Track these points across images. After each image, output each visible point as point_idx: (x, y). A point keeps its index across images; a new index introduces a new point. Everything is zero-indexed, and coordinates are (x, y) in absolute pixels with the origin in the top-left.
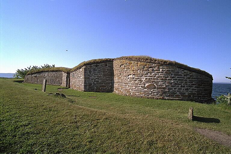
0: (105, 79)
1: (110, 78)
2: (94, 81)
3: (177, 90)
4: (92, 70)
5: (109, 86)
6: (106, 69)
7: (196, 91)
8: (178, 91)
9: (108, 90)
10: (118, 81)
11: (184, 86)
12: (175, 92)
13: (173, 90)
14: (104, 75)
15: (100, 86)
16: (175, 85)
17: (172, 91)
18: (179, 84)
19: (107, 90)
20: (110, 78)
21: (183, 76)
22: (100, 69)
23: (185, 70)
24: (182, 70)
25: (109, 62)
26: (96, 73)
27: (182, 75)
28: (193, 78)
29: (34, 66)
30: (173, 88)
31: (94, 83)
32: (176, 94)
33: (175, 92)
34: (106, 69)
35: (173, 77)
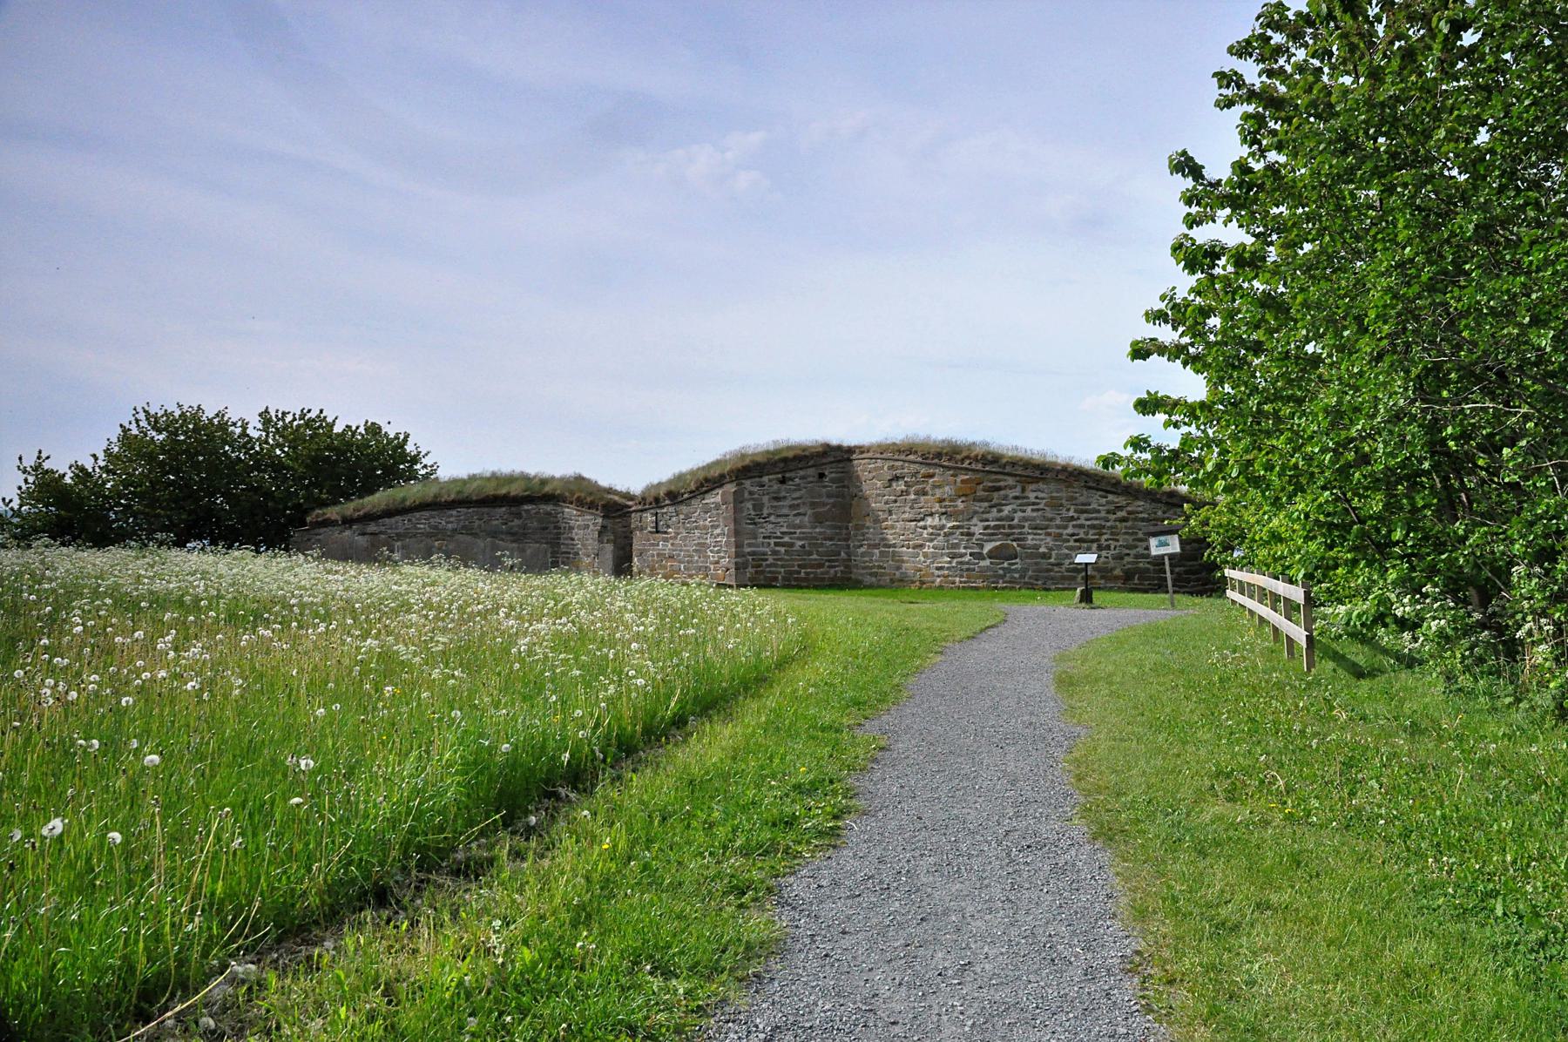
2: (776, 544)
4: (765, 499)
9: (832, 579)
11: (1108, 547)
14: (818, 519)
18: (1093, 541)
21: (1103, 514)
25: (832, 462)
26: (785, 511)
28: (1135, 519)
31: (775, 553)
35: (1072, 519)
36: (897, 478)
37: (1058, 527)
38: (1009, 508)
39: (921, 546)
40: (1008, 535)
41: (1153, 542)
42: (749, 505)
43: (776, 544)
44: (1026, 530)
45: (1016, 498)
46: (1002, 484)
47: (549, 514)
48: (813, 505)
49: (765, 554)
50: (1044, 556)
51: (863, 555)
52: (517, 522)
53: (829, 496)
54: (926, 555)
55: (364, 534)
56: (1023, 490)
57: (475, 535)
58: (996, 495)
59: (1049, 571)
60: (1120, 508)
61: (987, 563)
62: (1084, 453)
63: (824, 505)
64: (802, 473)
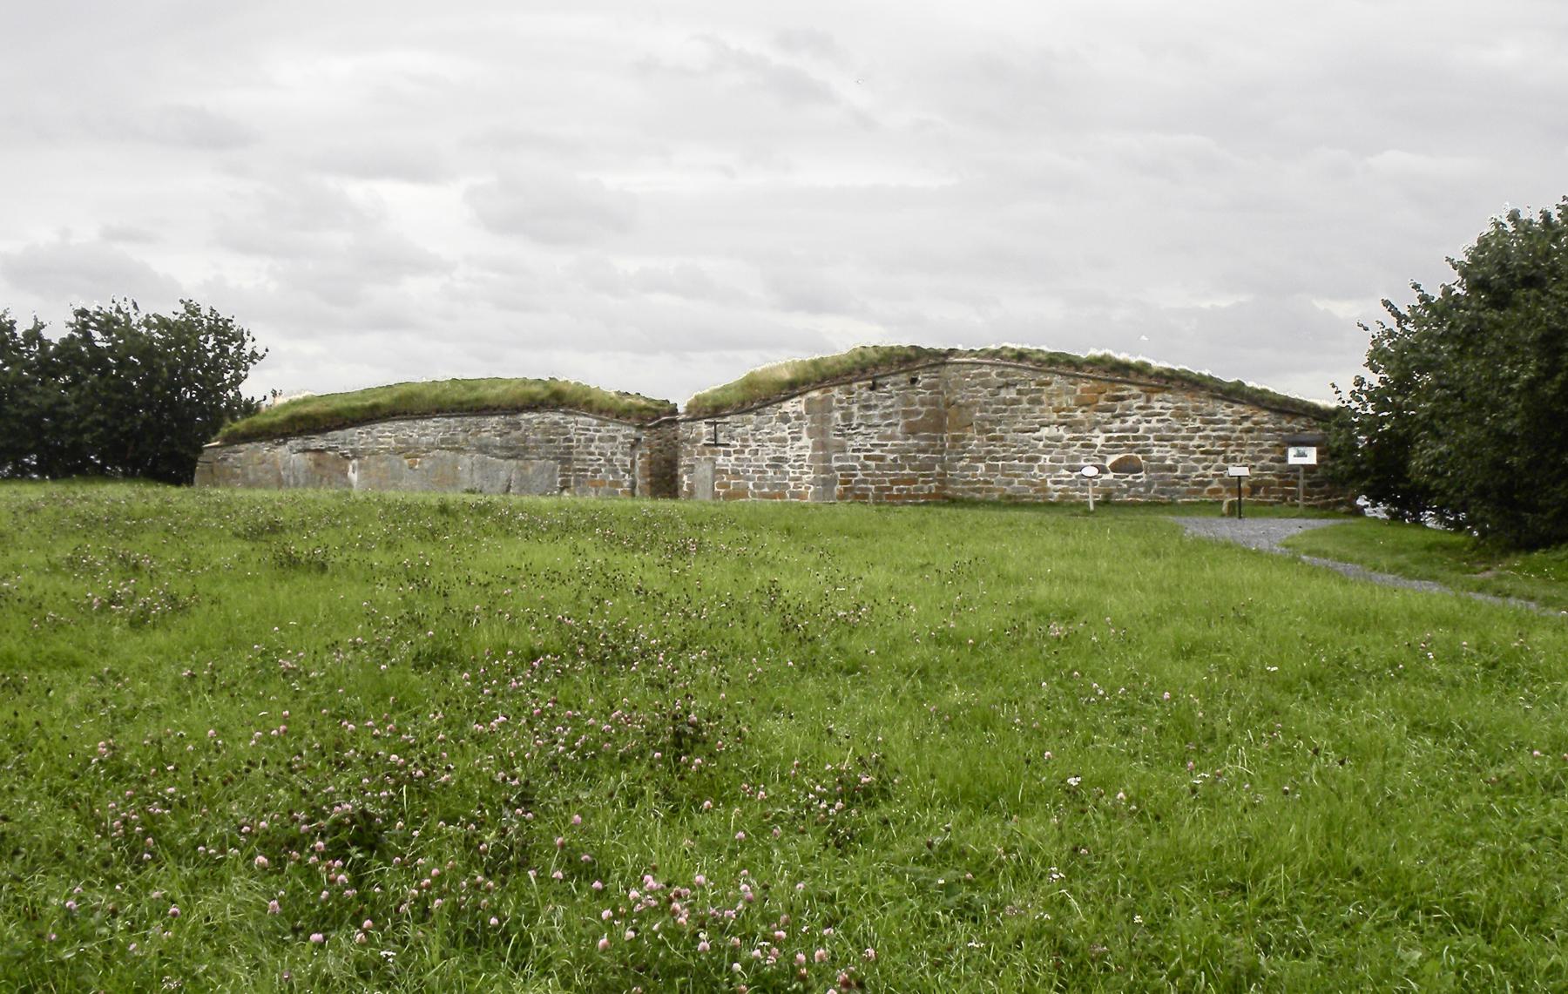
1: (934, 439)
2: (866, 458)
3: (1211, 472)
4: (855, 408)
6: (917, 398)
10: (989, 452)
14: (911, 430)
18: (1218, 453)
19: (925, 496)
20: (934, 439)
21: (1228, 425)
22: (889, 402)
26: (876, 421)
27: (1224, 422)
28: (1262, 430)
29: (1497, 224)
30: (1200, 467)
31: (865, 467)
34: (917, 398)
35: (1198, 430)
36: (1007, 385)
37: (1184, 438)
38: (1134, 418)
39: (1037, 459)
40: (1133, 446)
41: (1292, 451)
42: (837, 415)
43: (866, 458)
44: (1151, 441)
45: (1140, 408)
46: (1125, 393)
47: (556, 423)
48: (906, 414)
49: (854, 468)
50: (1171, 469)
51: (963, 469)
52: (515, 434)
53: (923, 403)
54: (1042, 469)
55: (306, 451)
56: (1148, 400)
57: (460, 450)
58: (1119, 405)
59: (1174, 484)
60: (1246, 418)
61: (1110, 476)
62: (1328, 401)
63: (919, 413)
64: (892, 379)
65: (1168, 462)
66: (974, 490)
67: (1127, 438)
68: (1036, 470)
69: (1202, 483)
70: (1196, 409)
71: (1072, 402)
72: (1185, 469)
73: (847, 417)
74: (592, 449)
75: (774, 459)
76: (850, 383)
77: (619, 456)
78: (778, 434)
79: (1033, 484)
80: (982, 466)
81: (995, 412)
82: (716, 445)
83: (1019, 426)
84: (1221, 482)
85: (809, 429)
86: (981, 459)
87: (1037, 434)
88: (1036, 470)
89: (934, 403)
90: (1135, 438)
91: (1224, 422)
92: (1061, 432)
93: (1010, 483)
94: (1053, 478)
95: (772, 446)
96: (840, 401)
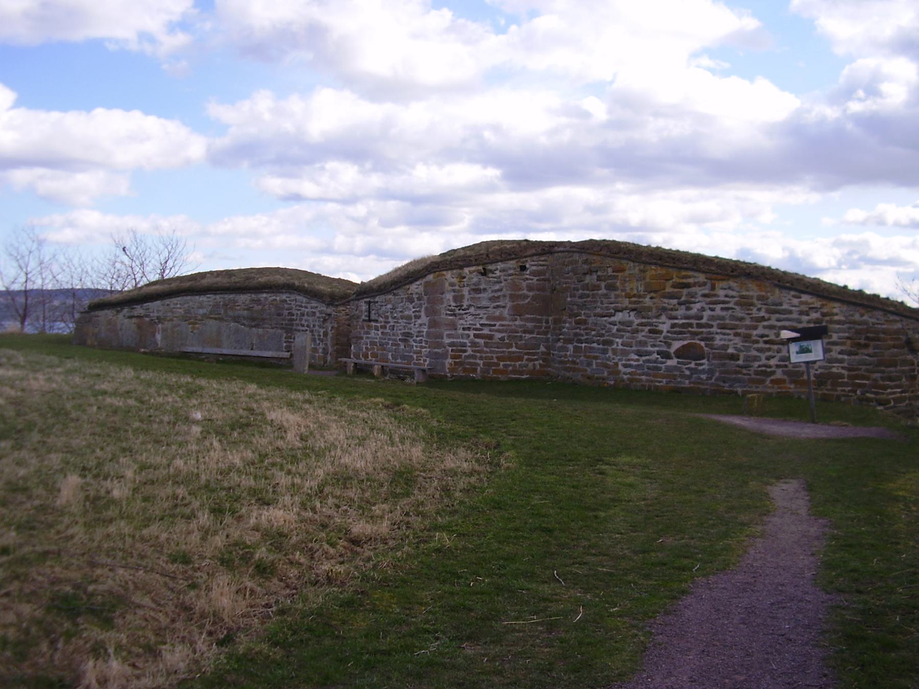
0: (521, 326)
2: (476, 336)
3: (773, 362)
5: (534, 354)
7: (843, 368)
8: (778, 366)
10: (576, 334)
12: (769, 370)
13: (764, 362)
14: (518, 312)
15: (497, 358)
16: (767, 346)
17: (759, 366)
20: (540, 321)
21: (795, 316)
22: (497, 287)
23: (802, 295)
24: (793, 293)
26: (484, 303)
27: (790, 312)
31: (474, 344)
32: (772, 378)
33: (769, 370)
34: (524, 284)
35: (763, 319)
36: (590, 272)
38: (698, 306)
40: (696, 334)
42: (449, 296)
43: (476, 336)
45: (704, 296)
46: (691, 280)
48: (513, 297)
49: (464, 345)
53: (530, 288)
55: (131, 317)
58: (685, 291)
64: (500, 266)
65: (730, 351)
66: (566, 369)
67: (691, 325)
68: (610, 354)
69: (764, 373)
70: (760, 298)
71: (641, 288)
72: (747, 359)
73: (458, 299)
74: (303, 322)
75: (403, 334)
76: (461, 268)
77: (317, 328)
78: (406, 313)
79: (607, 366)
80: (570, 347)
81: (581, 297)
82: (370, 321)
83: (598, 310)
84: (784, 373)
85: (426, 309)
86: (570, 341)
87: (613, 319)
88: (610, 354)
89: (542, 289)
90: (699, 326)
91: (790, 312)
92: (632, 318)
93: (589, 364)
94: (626, 363)
95: (402, 322)
96: (452, 285)
